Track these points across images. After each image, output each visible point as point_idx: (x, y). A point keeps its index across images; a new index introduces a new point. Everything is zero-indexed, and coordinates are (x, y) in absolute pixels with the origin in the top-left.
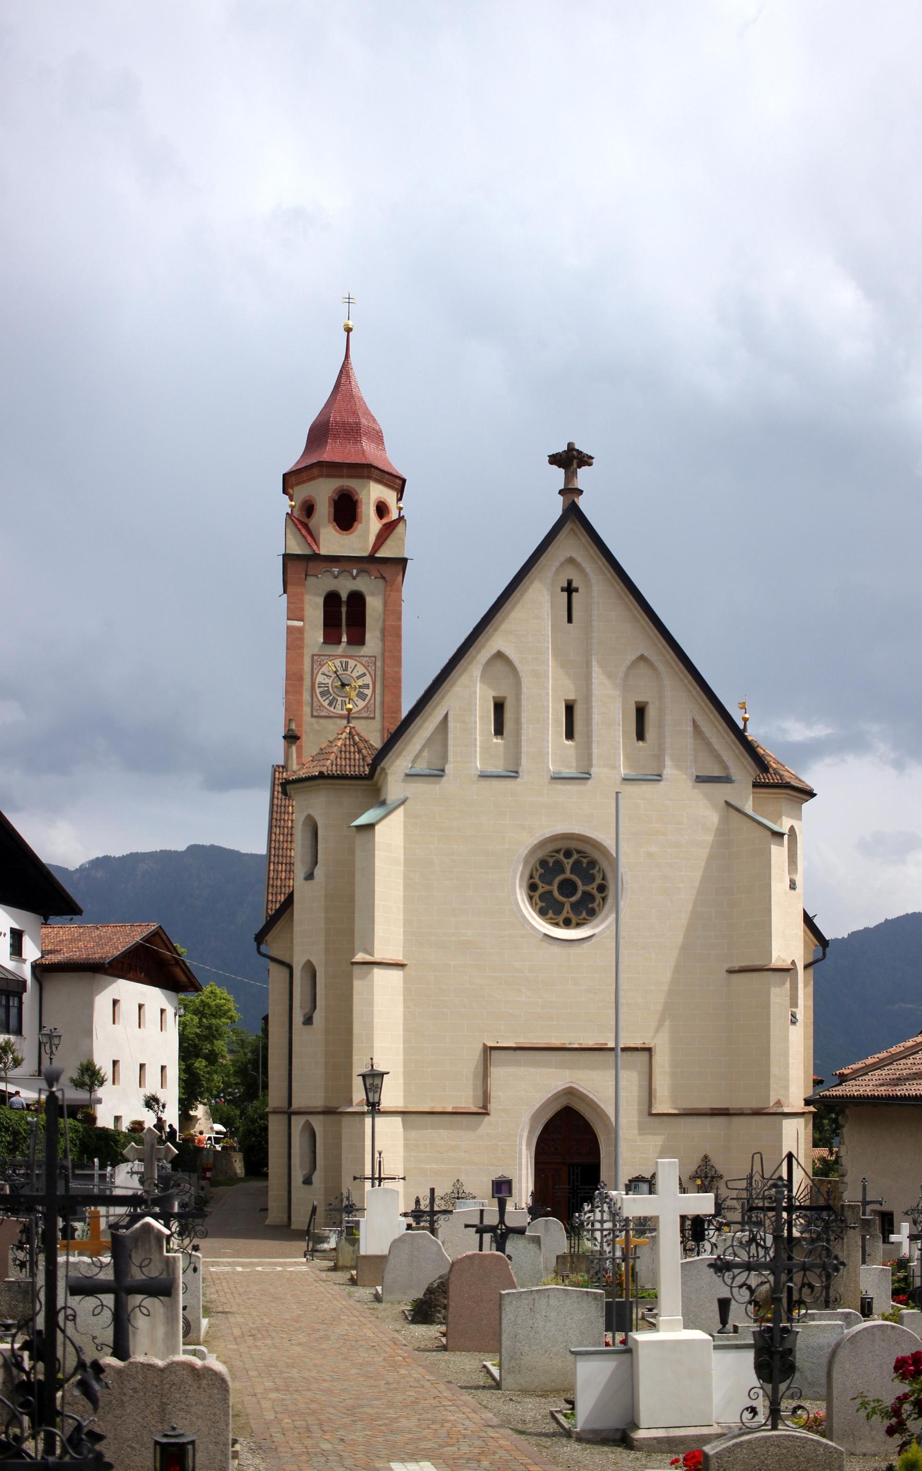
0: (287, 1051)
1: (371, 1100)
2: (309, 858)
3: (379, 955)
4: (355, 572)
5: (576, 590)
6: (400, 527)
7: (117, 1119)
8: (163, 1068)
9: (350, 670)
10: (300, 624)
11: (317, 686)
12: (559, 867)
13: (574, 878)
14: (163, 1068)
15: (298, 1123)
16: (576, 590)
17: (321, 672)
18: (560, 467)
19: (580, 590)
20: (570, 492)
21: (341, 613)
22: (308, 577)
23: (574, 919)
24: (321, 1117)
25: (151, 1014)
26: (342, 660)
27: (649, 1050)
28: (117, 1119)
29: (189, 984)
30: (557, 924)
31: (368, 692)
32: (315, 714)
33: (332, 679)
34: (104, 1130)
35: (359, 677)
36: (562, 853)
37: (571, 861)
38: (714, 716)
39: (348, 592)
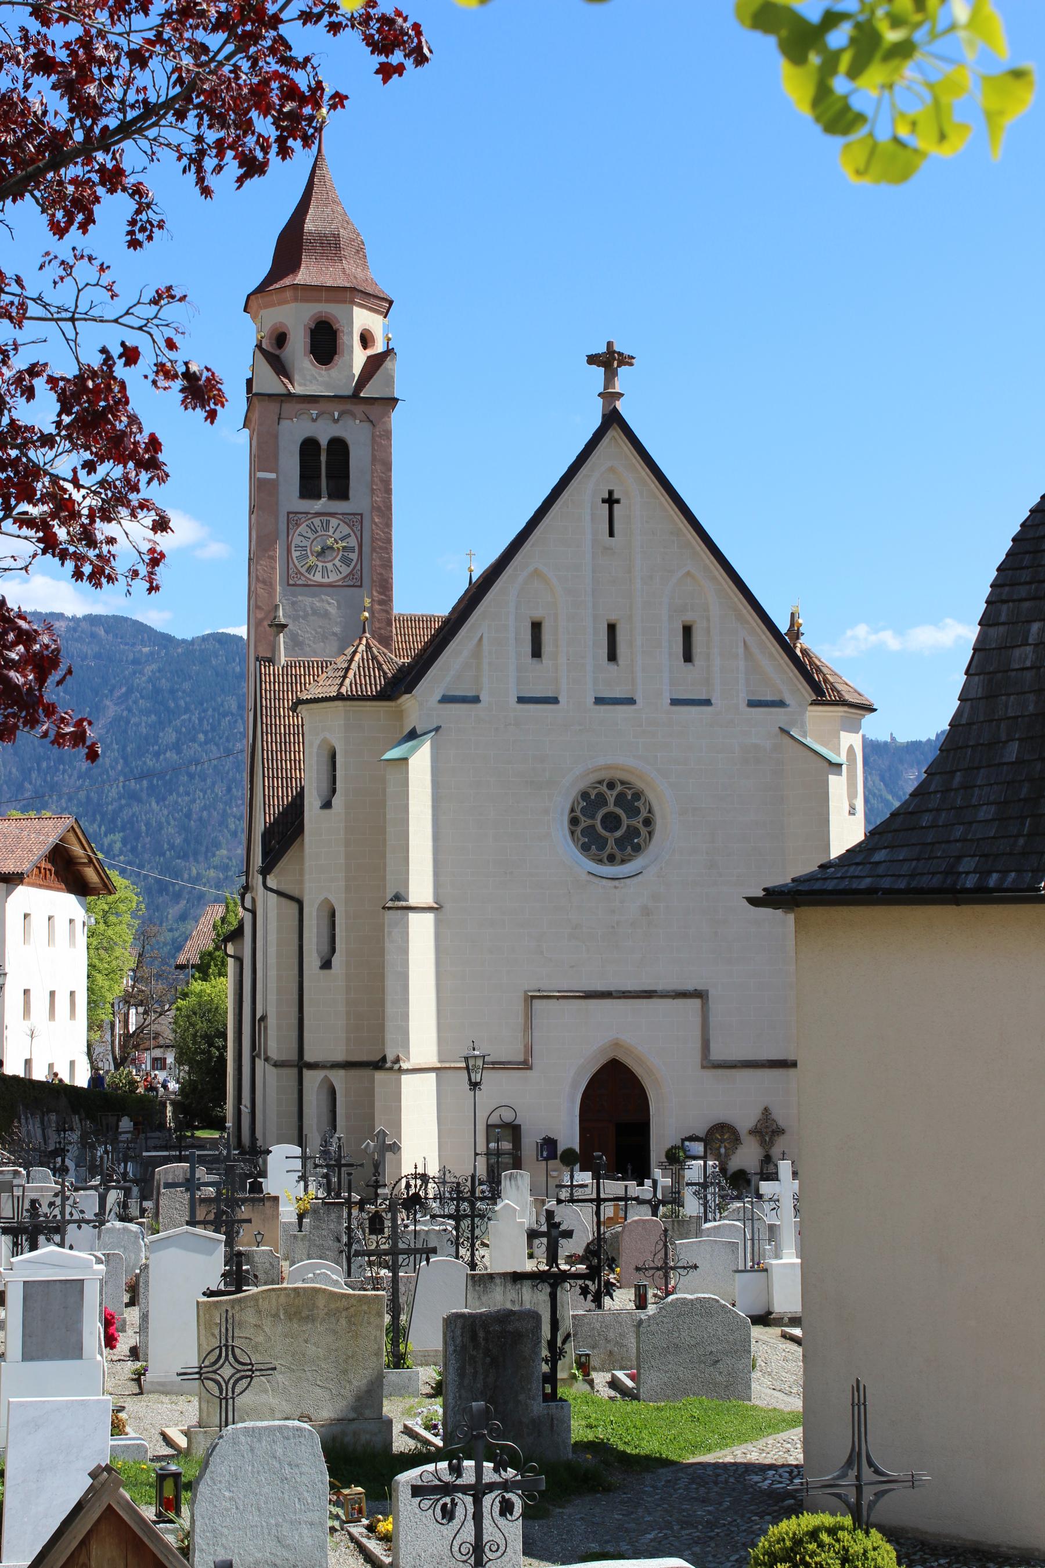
0: (295, 996)
1: (473, 1080)
2: (325, 785)
3: (413, 901)
4: (336, 414)
5: (618, 501)
6: (388, 363)
7: (28, 1063)
8: (72, 993)
9: (332, 530)
10: (273, 476)
11: (293, 548)
12: (601, 800)
13: (619, 811)
14: (72, 993)
15: (312, 1079)
16: (618, 501)
17: (297, 532)
18: (599, 366)
19: (622, 501)
20: (609, 397)
21: (320, 462)
22: (281, 420)
23: (619, 856)
24: (341, 1073)
25: (61, 926)
26: (322, 518)
27: (699, 994)
28: (28, 1063)
29: (101, 886)
30: (600, 861)
31: (354, 556)
32: (291, 582)
33: (310, 541)
34: (15, 1078)
35: (342, 539)
36: (605, 784)
37: (615, 793)
38: (767, 637)
39: (329, 438)
